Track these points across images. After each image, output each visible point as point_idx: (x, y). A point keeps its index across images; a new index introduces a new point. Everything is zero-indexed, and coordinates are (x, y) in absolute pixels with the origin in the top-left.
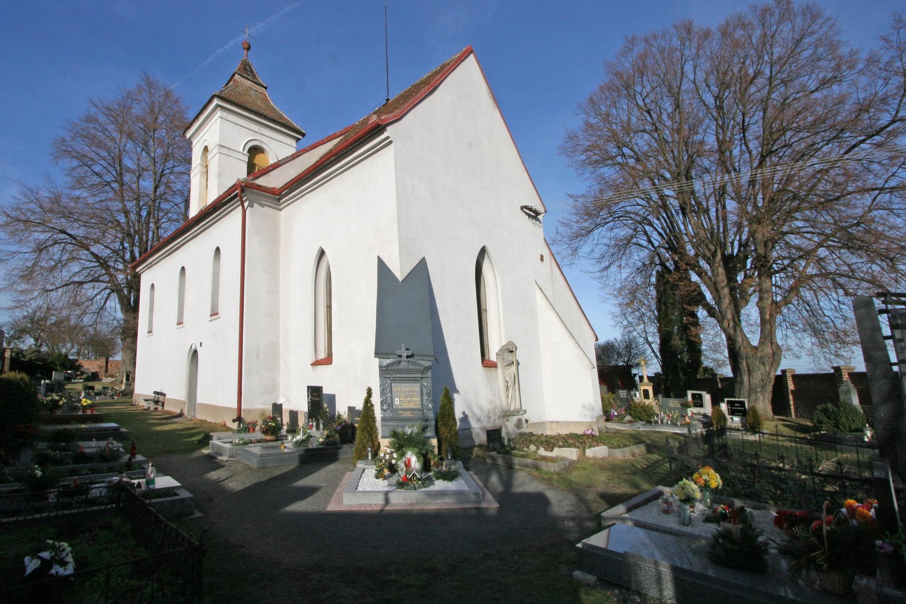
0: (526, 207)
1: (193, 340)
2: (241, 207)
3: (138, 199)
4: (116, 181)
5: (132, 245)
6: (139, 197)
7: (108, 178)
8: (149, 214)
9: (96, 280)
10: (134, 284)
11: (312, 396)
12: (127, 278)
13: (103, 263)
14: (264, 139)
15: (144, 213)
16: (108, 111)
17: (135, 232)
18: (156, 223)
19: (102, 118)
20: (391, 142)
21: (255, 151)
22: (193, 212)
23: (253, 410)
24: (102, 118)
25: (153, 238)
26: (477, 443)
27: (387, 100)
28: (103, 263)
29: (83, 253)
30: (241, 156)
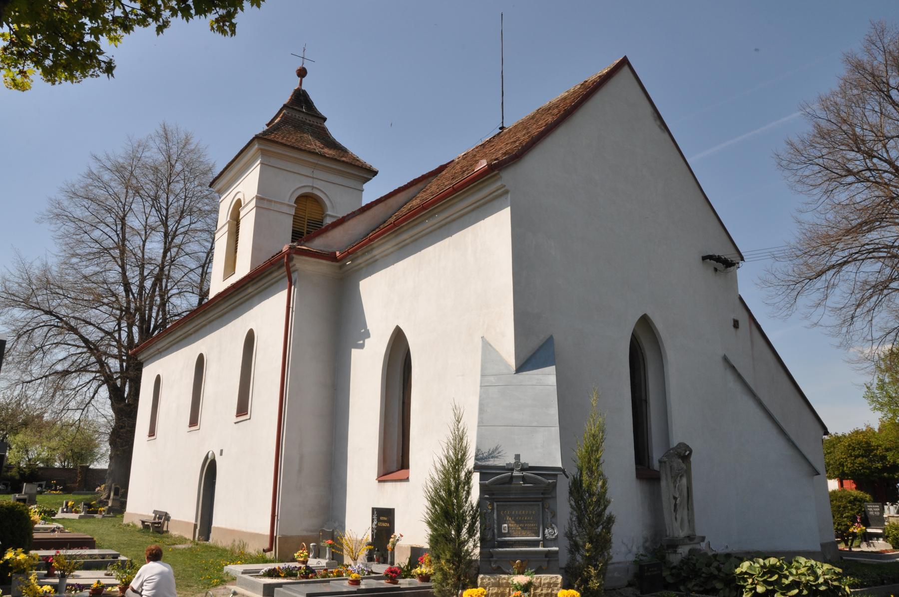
0: (711, 257)
1: (196, 436)
2: (287, 279)
3: (142, 267)
4: (118, 247)
5: (130, 327)
6: (143, 264)
7: (109, 243)
8: (154, 285)
9: (83, 370)
10: (133, 373)
11: (379, 520)
12: (121, 366)
13: (91, 347)
14: (318, 184)
15: (148, 284)
16: (119, 169)
17: (136, 309)
18: (162, 296)
19: (106, 176)
20: (507, 192)
21: (307, 200)
22: (217, 285)
23: (291, 537)
24: (106, 176)
25: (151, 310)
26: (234, 21)
27: (502, 128)
28: (91, 347)
29: (71, 337)
30: (285, 209)
